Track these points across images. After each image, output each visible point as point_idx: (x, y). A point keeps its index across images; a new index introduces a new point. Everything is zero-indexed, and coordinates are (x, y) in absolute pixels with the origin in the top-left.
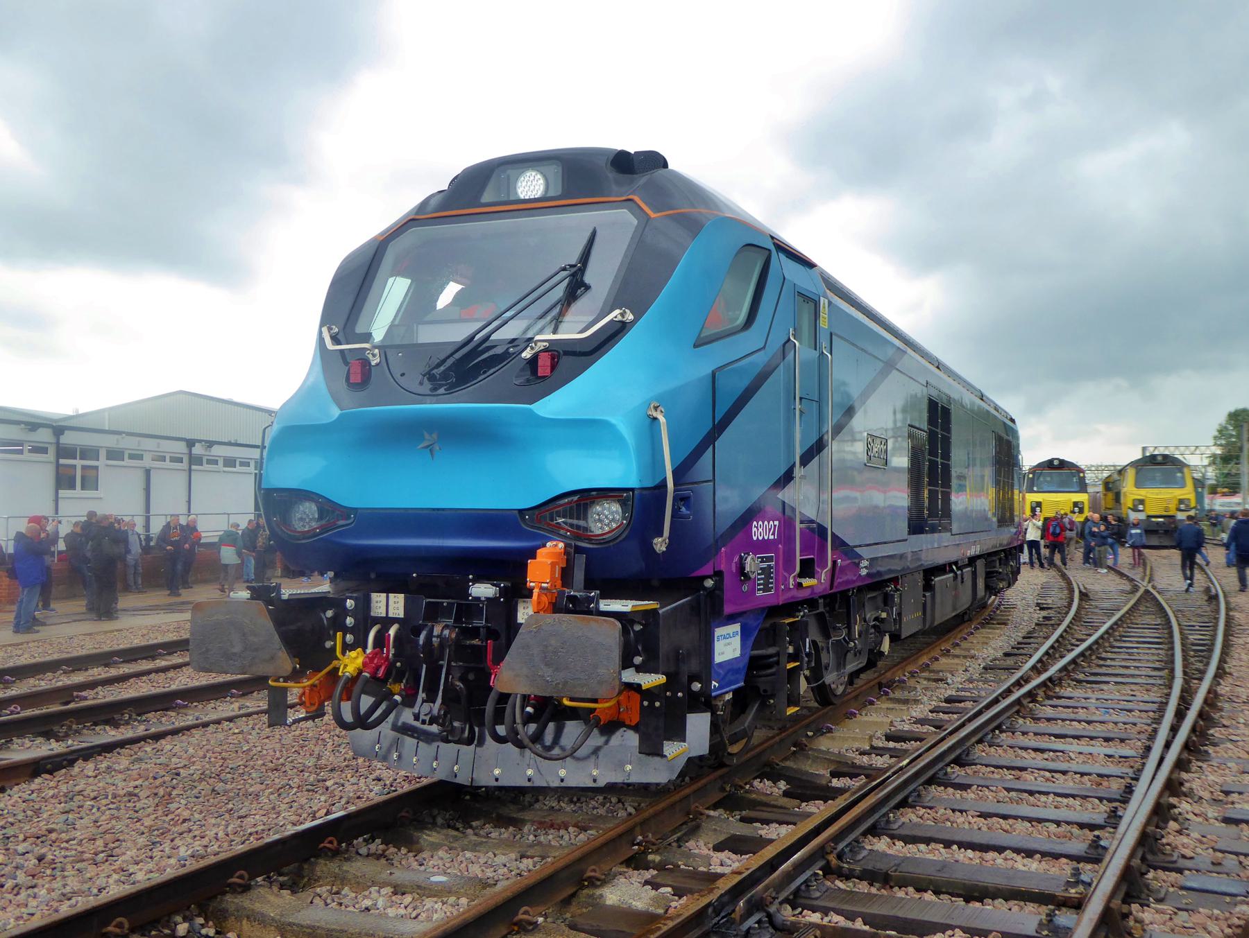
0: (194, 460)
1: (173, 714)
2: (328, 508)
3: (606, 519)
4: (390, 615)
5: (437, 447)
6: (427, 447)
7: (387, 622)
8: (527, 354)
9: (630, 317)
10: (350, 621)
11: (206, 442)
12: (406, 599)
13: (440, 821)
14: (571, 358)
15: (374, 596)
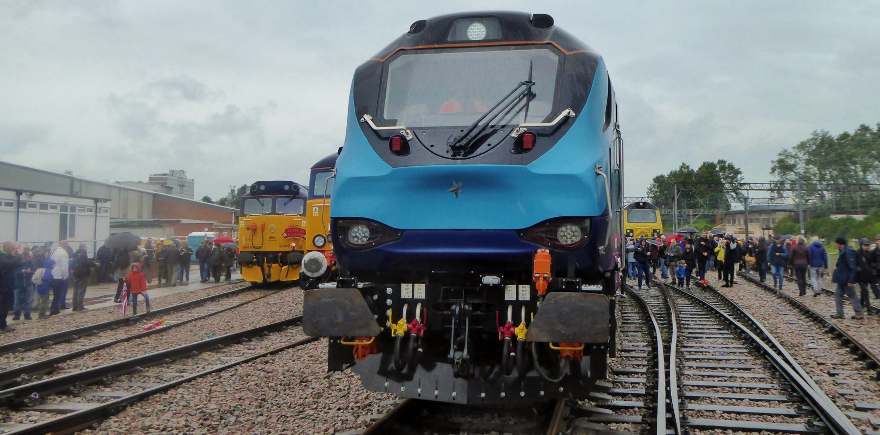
0: (21, 205)
2: (376, 227)
3: (569, 235)
4: (416, 297)
5: (460, 191)
7: (412, 303)
8: (514, 135)
9: (573, 114)
10: (389, 302)
11: (29, 192)
14: (541, 138)
15: (403, 286)
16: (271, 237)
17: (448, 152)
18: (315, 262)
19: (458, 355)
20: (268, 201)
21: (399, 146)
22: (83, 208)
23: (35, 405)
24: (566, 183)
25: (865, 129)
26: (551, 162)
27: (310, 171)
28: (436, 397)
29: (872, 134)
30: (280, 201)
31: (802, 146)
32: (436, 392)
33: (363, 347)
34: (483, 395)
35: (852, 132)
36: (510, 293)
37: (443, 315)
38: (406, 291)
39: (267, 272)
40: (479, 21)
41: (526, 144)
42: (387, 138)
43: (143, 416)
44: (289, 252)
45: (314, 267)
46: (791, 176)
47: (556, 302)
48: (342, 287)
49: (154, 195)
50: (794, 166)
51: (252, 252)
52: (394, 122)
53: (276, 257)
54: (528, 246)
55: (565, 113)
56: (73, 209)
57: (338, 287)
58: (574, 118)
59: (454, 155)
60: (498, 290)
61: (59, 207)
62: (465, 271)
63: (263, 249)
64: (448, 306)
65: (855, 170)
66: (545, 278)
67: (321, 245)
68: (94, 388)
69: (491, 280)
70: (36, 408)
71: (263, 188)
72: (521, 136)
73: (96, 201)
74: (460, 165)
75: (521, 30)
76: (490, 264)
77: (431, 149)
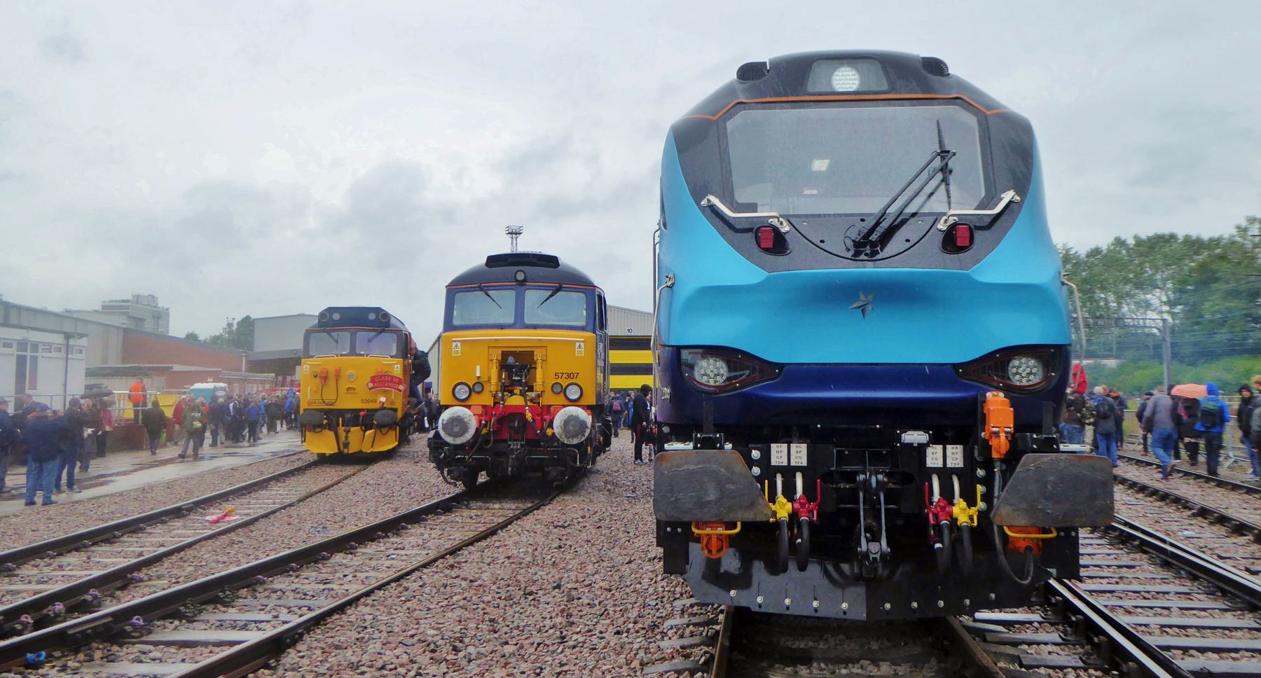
3: (1026, 372)
4: (793, 464)
5: (869, 307)
7: (789, 472)
8: (942, 226)
9: (1018, 198)
13: (98, 654)
15: (773, 446)
17: (848, 250)
18: (458, 421)
19: (874, 547)
20: (345, 336)
21: (772, 242)
22: (49, 347)
23: (142, 636)
25: (1119, 242)
26: (999, 265)
27: (444, 290)
28: (816, 610)
29: (1128, 249)
30: (362, 335)
32: (815, 604)
33: (719, 537)
34: (888, 606)
35: (1104, 247)
36: (934, 457)
37: (838, 489)
38: (779, 454)
39: (342, 439)
40: (849, 65)
41: (956, 240)
42: (750, 230)
43: (337, 647)
44: (376, 410)
45: (456, 429)
47: (1037, 468)
49: (125, 330)
51: (321, 410)
52: (753, 207)
53: (357, 417)
54: (973, 387)
55: (1008, 196)
56: (35, 346)
57: (695, 448)
58: (1020, 204)
59: (857, 254)
60: (921, 449)
61: (15, 346)
62: (857, 425)
63: (339, 406)
64: (851, 477)
65: (1106, 300)
68: (210, 607)
69: (914, 437)
70: (144, 639)
71: (336, 317)
72: (953, 227)
73: (68, 336)
74: (868, 269)
75: (915, 79)
76: (913, 415)
77: (821, 245)
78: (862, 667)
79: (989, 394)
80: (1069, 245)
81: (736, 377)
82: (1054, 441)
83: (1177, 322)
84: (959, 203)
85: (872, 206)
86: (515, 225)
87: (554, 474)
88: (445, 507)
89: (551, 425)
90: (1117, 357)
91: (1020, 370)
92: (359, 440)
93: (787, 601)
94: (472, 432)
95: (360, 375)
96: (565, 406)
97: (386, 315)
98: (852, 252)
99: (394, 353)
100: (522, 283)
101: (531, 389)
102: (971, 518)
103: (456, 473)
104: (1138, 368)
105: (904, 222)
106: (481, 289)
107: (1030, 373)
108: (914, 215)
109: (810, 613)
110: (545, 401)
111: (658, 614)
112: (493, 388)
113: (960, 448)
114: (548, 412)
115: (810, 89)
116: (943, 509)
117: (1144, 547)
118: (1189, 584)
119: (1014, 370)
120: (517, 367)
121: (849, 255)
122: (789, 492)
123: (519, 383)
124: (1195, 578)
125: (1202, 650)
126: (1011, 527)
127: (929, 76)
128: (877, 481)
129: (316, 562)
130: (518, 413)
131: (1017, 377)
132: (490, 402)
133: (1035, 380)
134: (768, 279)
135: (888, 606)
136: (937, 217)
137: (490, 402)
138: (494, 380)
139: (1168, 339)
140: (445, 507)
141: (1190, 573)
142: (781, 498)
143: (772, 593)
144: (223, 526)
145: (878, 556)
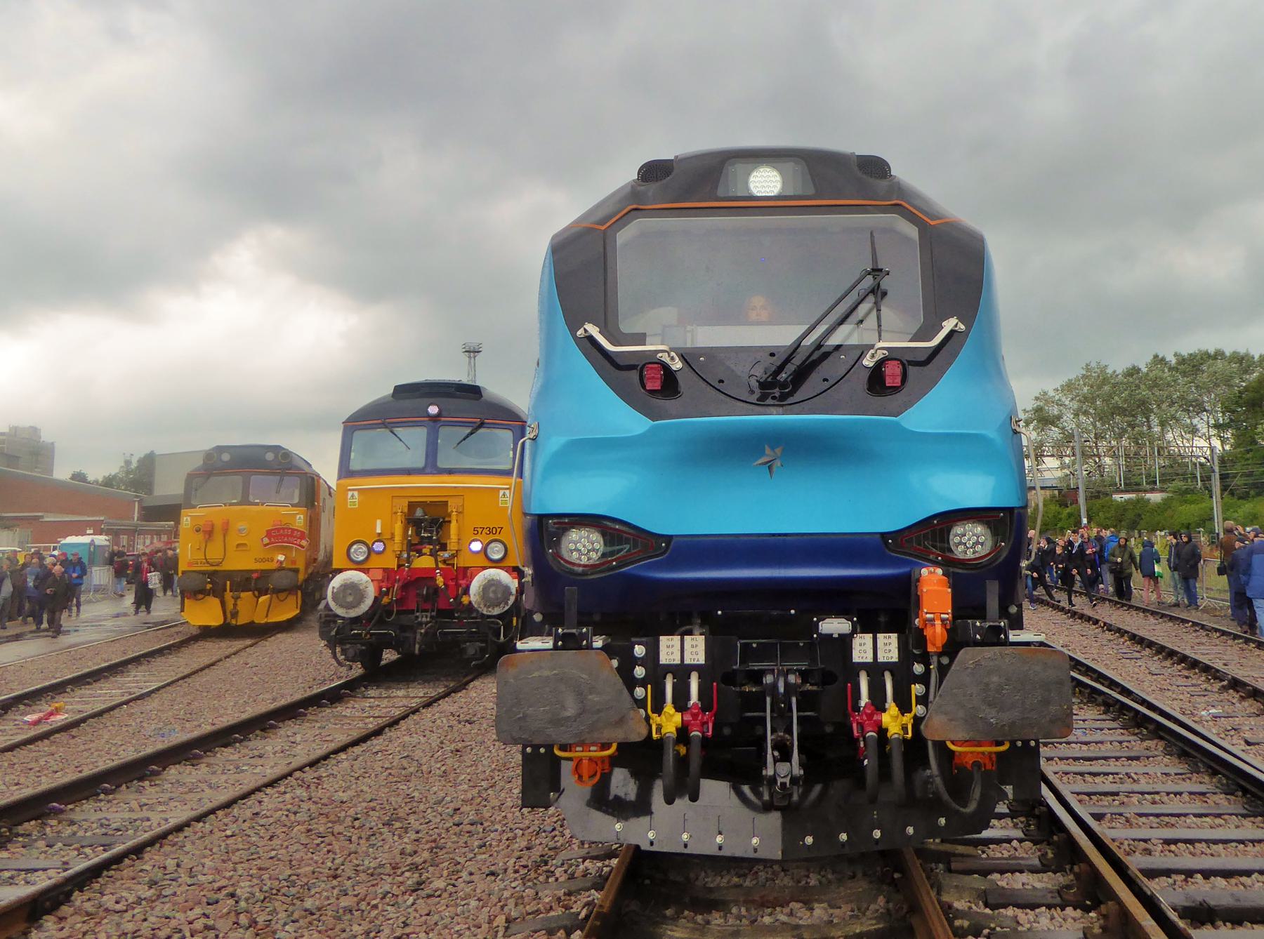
1: (54, 822)
3: (971, 541)
4: (687, 661)
5: (778, 463)
6: (766, 463)
7: (681, 672)
8: (868, 362)
9: (962, 327)
12: (899, 639)
15: (663, 640)
16: (238, 545)
17: (752, 392)
18: (350, 587)
19: (783, 768)
24: (957, 447)
25: (1159, 361)
26: (929, 413)
31: (1069, 387)
32: (719, 839)
34: (809, 840)
36: (862, 649)
37: (742, 694)
38: (670, 649)
39: (230, 606)
45: (350, 599)
46: (1055, 432)
47: (977, 664)
48: (563, 648)
50: (1059, 417)
51: (203, 573)
52: (640, 339)
55: (949, 325)
57: (556, 648)
58: (965, 334)
59: (763, 398)
60: (845, 642)
62: (768, 610)
64: (757, 677)
66: (943, 620)
67: (361, 558)
69: (834, 626)
71: (226, 457)
72: (880, 364)
75: (845, 181)
76: (833, 598)
77: (832, 382)
78: (791, 914)
79: (924, 571)
80: (1103, 363)
81: (612, 553)
82: (997, 630)
83: (1227, 447)
84: (885, 334)
85: (783, 336)
86: (473, 341)
87: (471, 651)
88: (334, 697)
89: (466, 591)
90: (1162, 491)
91: (964, 540)
92: (252, 609)
93: (685, 837)
94: (368, 602)
95: (244, 533)
96: (484, 568)
97: (287, 455)
98: (756, 396)
99: (296, 501)
100: (435, 419)
101: (444, 547)
102: (904, 728)
103: (351, 653)
104: (1186, 502)
105: (826, 355)
106: (384, 425)
107: (977, 543)
108: (838, 347)
109: (713, 851)
110: (461, 562)
111: (551, 844)
112: (397, 547)
113: (894, 636)
114: (465, 576)
115: (721, 192)
116: (870, 716)
117: (1159, 732)
118: (1207, 779)
119: (957, 540)
120: (428, 523)
121: (753, 398)
122: (681, 702)
123: (430, 541)
124: (1214, 773)
125: (1207, 874)
126: (953, 742)
127: (871, 180)
128: (787, 684)
129: (141, 779)
130: (426, 577)
131: (961, 548)
132: (393, 564)
133: (982, 551)
134: (652, 430)
135: (809, 840)
136: (863, 350)
137: (393, 564)
138: (398, 538)
139: (1217, 469)
140: (334, 697)
141: (1211, 767)
142: (669, 708)
143: (671, 827)
144: (44, 728)
145: (787, 780)
